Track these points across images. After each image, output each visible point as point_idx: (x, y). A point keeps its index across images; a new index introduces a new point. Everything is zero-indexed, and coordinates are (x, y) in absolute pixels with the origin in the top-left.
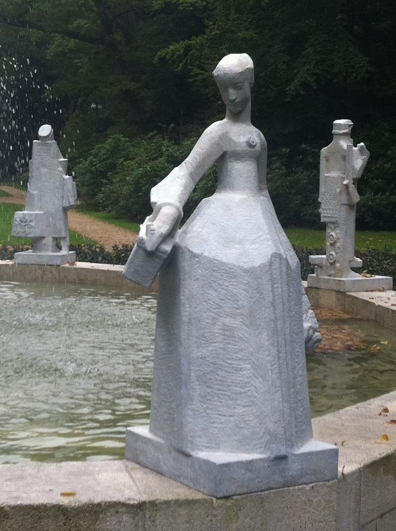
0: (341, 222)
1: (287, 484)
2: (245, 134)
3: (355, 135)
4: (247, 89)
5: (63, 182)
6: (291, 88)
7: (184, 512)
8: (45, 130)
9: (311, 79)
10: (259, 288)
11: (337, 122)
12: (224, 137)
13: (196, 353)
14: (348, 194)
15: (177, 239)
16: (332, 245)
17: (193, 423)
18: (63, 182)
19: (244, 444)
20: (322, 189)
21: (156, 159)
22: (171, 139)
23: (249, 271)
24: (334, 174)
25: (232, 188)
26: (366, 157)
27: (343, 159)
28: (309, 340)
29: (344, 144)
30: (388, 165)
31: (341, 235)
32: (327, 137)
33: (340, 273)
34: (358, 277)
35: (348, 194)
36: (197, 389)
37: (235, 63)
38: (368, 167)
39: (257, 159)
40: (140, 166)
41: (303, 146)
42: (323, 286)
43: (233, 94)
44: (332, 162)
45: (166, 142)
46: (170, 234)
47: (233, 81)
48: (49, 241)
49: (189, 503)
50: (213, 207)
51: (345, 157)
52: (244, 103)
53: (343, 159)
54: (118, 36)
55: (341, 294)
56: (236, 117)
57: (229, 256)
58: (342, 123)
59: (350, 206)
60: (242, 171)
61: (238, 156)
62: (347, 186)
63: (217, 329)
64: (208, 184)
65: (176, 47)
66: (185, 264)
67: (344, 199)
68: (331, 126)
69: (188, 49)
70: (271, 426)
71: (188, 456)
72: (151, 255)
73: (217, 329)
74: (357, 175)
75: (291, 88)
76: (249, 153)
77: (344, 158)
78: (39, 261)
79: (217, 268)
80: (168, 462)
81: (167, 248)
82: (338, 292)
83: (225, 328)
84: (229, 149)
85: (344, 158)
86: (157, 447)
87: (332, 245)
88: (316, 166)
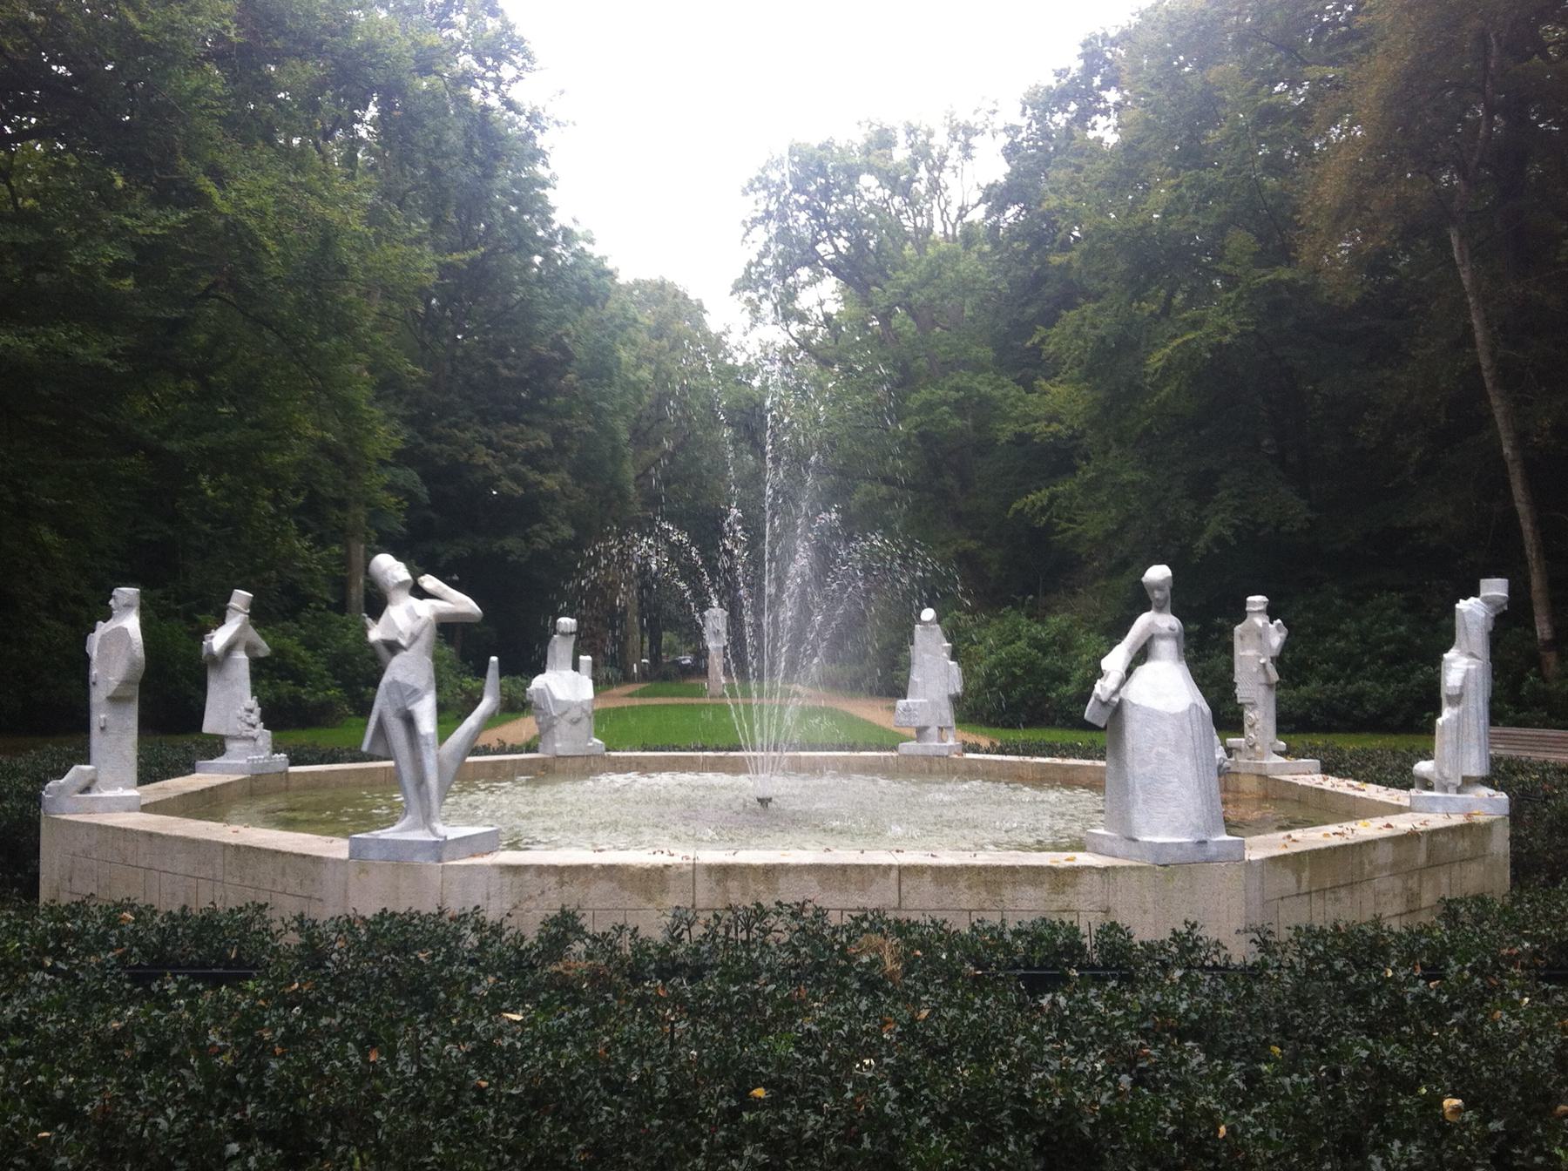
0: (1260, 702)
1: (1207, 861)
2: (1167, 621)
3: (1272, 613)
4: (1168, 591)
5: (948, 669)
6: (1201, 544)
7: (1135, 874)
8: (928, 614)
9: (1227, 533)
10: (1182, 728)
11: (1250, 599)
12: (1152, 624)
13: (1138, 770)
14: (1266, 673)
15: (1122, 694)
16: (1251, 726)
17: (1138, 818)
18: (948, 669)
19: (1175, 831)
20: (1237, 668)
21: (1013, 642)
22: (1029, 616)
23: (1175, 715)
24: (1250, 653)
25: (1158, 658)
26: (1284, 634)
27: (1259, 638)
28: (1220, 766)
29: (1260, 621)
30: (1342, 644)
31: (1260, 716)
32: (1241, 614)
33: (1261, 755)
34: (1282, 760)
35: (1266, 673)
36: (1140, 796)
37: (1158, 573)
38: (1287, 646)
39: (1177, 638)
40: (991, 653)
41: (1219, 620)
42: (1243, 771)
43: (1157, 594)
44: (1247, 640)
45: (1024, 620)
46: (1116, 692)
47: (1158, 586)
48: (933, 731)
49: (1139, 868)
50: (1144, 672)
51: (1261, 635)
52: (1165, 601)
53: (1259, 638)
54: (949, 480)
55: (1263, 777)
56: (1160, 610)
57: (1159, 705)
58: (1257, 601)
59: (1270, 686)
60: (1166, 649)
61: (1162, 637)
62: (1264, 665)
63: (1153, 755)
64: (1142, 655)
65: (1039, 497)
66: (1128, 712)
67: (1262, 679)
68: (1244, 604)
69: (1053, 498)
70: (1195, 821)
71: (1135, 840)
72: (1104, 704)
73: (1153, 755)
74: (1276, 653)
75: (1201, 544)
76: (1171, 634)
77: (1260, 636)
78: (925, 752)
79: (1152, 715)
80: (1121, 847)
81: (1116, 699)
82: (1259, 776)
83: (1158, 754)
84: (1155, 631)
85: (1260, 636)
86: (1112, 840)
87: (1251, 726)
88: (1229, 649)
